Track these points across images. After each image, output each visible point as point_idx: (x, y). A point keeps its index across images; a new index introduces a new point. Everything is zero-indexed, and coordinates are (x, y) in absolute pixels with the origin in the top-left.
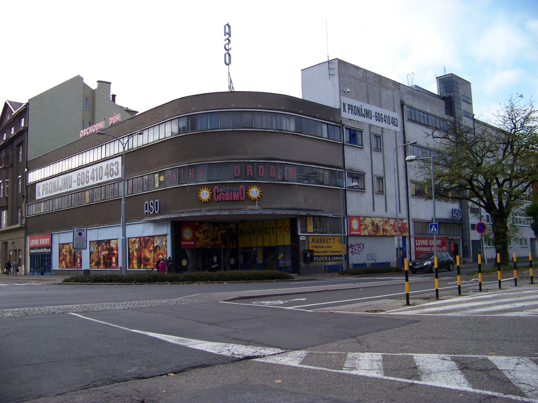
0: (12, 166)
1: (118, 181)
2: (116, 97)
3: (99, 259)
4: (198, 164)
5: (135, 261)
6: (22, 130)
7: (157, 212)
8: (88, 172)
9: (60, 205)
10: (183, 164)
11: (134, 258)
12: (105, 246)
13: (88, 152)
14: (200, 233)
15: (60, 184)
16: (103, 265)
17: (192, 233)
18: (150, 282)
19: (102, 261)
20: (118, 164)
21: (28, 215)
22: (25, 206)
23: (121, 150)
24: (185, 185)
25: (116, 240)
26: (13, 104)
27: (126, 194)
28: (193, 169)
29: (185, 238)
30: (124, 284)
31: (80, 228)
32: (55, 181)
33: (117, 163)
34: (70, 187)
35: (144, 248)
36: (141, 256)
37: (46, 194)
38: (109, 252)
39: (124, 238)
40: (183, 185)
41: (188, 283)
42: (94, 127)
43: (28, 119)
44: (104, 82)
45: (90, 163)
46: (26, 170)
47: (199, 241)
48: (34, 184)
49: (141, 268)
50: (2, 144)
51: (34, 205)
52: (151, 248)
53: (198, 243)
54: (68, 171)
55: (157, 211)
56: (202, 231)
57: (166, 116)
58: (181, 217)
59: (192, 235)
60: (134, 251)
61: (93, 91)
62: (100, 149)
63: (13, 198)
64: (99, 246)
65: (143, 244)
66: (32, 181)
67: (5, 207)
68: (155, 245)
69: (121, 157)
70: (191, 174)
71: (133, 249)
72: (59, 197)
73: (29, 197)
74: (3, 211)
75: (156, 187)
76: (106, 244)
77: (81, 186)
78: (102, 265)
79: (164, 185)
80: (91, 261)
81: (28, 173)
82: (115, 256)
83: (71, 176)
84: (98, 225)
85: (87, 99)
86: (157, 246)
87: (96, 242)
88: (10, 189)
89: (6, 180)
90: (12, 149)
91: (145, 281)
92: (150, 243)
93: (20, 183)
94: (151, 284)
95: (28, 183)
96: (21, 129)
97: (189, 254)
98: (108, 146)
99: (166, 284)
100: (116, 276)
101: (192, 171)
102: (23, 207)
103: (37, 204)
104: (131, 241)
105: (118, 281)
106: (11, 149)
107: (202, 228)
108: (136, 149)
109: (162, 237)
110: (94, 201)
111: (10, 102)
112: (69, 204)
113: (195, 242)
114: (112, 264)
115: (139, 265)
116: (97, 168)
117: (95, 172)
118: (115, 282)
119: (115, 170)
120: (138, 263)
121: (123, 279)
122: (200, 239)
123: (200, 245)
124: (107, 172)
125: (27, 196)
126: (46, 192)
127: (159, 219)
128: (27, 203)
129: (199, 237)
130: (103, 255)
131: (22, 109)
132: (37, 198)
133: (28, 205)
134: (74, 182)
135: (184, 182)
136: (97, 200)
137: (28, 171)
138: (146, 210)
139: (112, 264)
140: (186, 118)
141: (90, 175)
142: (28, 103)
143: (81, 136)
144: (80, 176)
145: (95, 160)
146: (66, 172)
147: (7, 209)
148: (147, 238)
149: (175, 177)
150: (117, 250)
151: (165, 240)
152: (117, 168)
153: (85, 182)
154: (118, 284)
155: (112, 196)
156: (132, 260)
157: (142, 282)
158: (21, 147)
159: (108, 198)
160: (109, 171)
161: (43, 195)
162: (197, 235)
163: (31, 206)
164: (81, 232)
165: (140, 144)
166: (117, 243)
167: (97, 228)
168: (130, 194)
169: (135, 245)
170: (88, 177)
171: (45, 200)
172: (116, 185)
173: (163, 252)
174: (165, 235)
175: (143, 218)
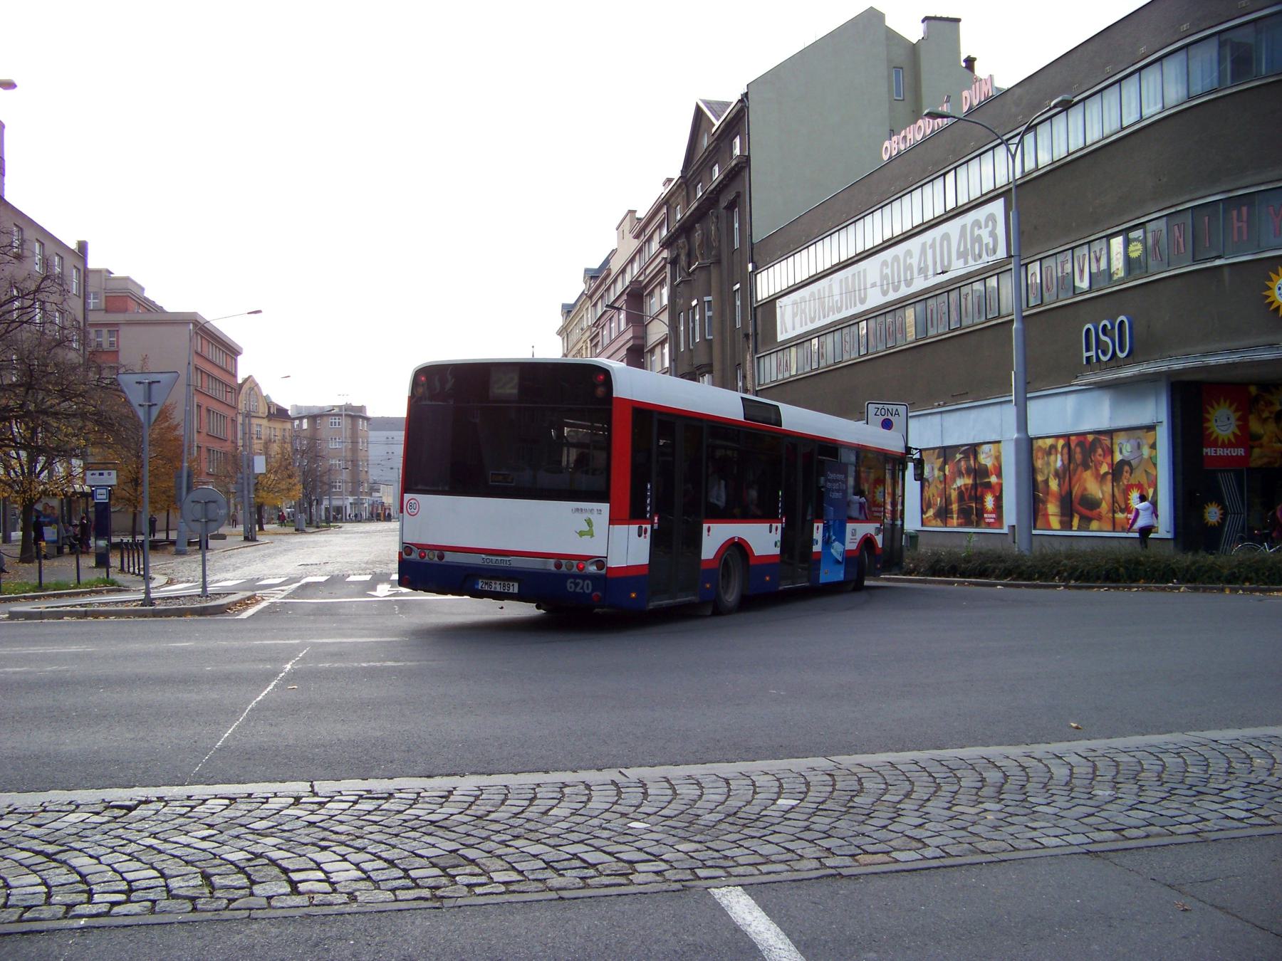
0: (718, 262)
1: (996, 269)
2: (976, 63)
3: (948, 501)
4: (1263, 188)
5: (1052, 508)
6: (736, 165)
7: (1121, 355)
8: (909, 253)
9: (838, 351)
10: (1209, 195)
11: (1050, 498)
12: (963, 463)
13: (906, 199)
14: (1264, 421)
15: (837, 298)
16: (958, 519)
17: (1238, 419)
18: (1114, 581)
19: (955, 507)
20: (994, 221)
21: (759, 385)
22: (752, 361)
23: (1002, 180)
24: (1218, 262)
25: (996, 445)
26: (714, 107)
27: (1024, 306)
28: (1244, 209)
29: (1214, 436)
30: (1027, 586)
31: (886, 407)
32: (824, 288)
33: (991, 217)
34: (863, 301)
35: (1080, 469)
36: (1071, 492)
37: (801, 326)
38: (975, 479)
39: (1022, 436)
40: (1208, 265)
41: (1252, 591)
42: (920, 127)
43: (749, 134)
44: (941, 19)
45: (914, 228)
46: (750, 267)
47: (1261, 446)
48: (771, 302)
49: (1070, 528)
50: (695, 209)
51: (774, 356)
52: (1104, 469)
53: (1257, 451)
54: (856, 259)
55: (1122, 350)
56: (1271, 413)
57: (1143, 50)
58: (1207, 368)
59: (1238, 427)
60: (1051, 476)
61: (914, 49)
62: (939, 182)
63: (723, 341)
64: (945, 463)
65: (1078, 457)
66: (765, 296)
67: (705, 366)
68: (1118, 457)
69: (1002, 199)
70: (1236, 224)
71: (1046, 472)
72: (834, 331)
73: (759, 337)
74: (703, 376)
75: (1115, 277)
76: (967, 457)
77: (892, 296)
78: (955, 516)
79: (1144, 270)
80: (925, 506)
81: (756, 275)
82: (993, 493)
83: (865, 270)
84: (941, 403)
85: (898, 68)
86: (1123, 462)
87: (937, 451)
88: (716, 323)
89: (706, 299)
90: (717, 218)
91: (1098, 578)
92: (1100, 451)
93: (738, 303)
94: (1118, 588)
95: (757, 301)
96: (733, 163)
97: (1227, 483)
98: (962, 172)
99: (1172, 589)
100: (1000, 558)
101: (1239, 213)
102: (748, 364)
103: (780, 354)
104: (1040, 447)
105: (1007, 573)
106: (714, 220)
107: (1271, 404)
108: (1048, 168)
109: (1140, 433)
110: (929, 335)
111: (707, 103)
112: (861, 349)
113: (1249, 450)
114: (985, 515)
115: (1066, 519)
116: (934, 239)
117: (929, 253)
118: (997, 578)
119: (987, 239)
120: (1063, 514)
121: (1024, 568)
122: (1265, 440)
123: (1265, 460)
124: (962, 249)
125: (756, 334)
126: (801, 319)
127: (1130, 377)
128: (756, 352)
129: (1262, 432)
130: (959, 488)
131: (734, 110)
132: (780, 338)
133: (759, 358)
134: (873, 285)
135: (1214, 254)
136: (937, 330)
137: (756, 268)
138: (1088, 350)
139: (985, 515)
140: (1215, 41)
141: (914, 261)
142: (747, 93)
143: (886, 157)
144: (887, 268)
145: (928, 217)
146: (849, 262)
147: (710, 372)
148: (1090, 438)
149: (1181, 240)
150: (999, 475)
151: (1151, 442)
152: (993, 235)
153: (903, 283)
154: (1005, 585)
155: (979, 317)
156: (1045, 502)
157: (1088, 581)
158: (737, 209)
159: (970, 322)
160: (969, 246)
161: (794, 329)
162: (1255, 426)
163: (767, 359)
164: (890, 417)
165: (1060, 152)
166: (999, 452)
167: (941, 413)
168: (1034, 307)
169: (1052, 458)
170: (909, 267)
171: (801, 341)
172: (993, 282)
173: (1144, 481)
174: (1151, 428)
175: (1077, 377)
